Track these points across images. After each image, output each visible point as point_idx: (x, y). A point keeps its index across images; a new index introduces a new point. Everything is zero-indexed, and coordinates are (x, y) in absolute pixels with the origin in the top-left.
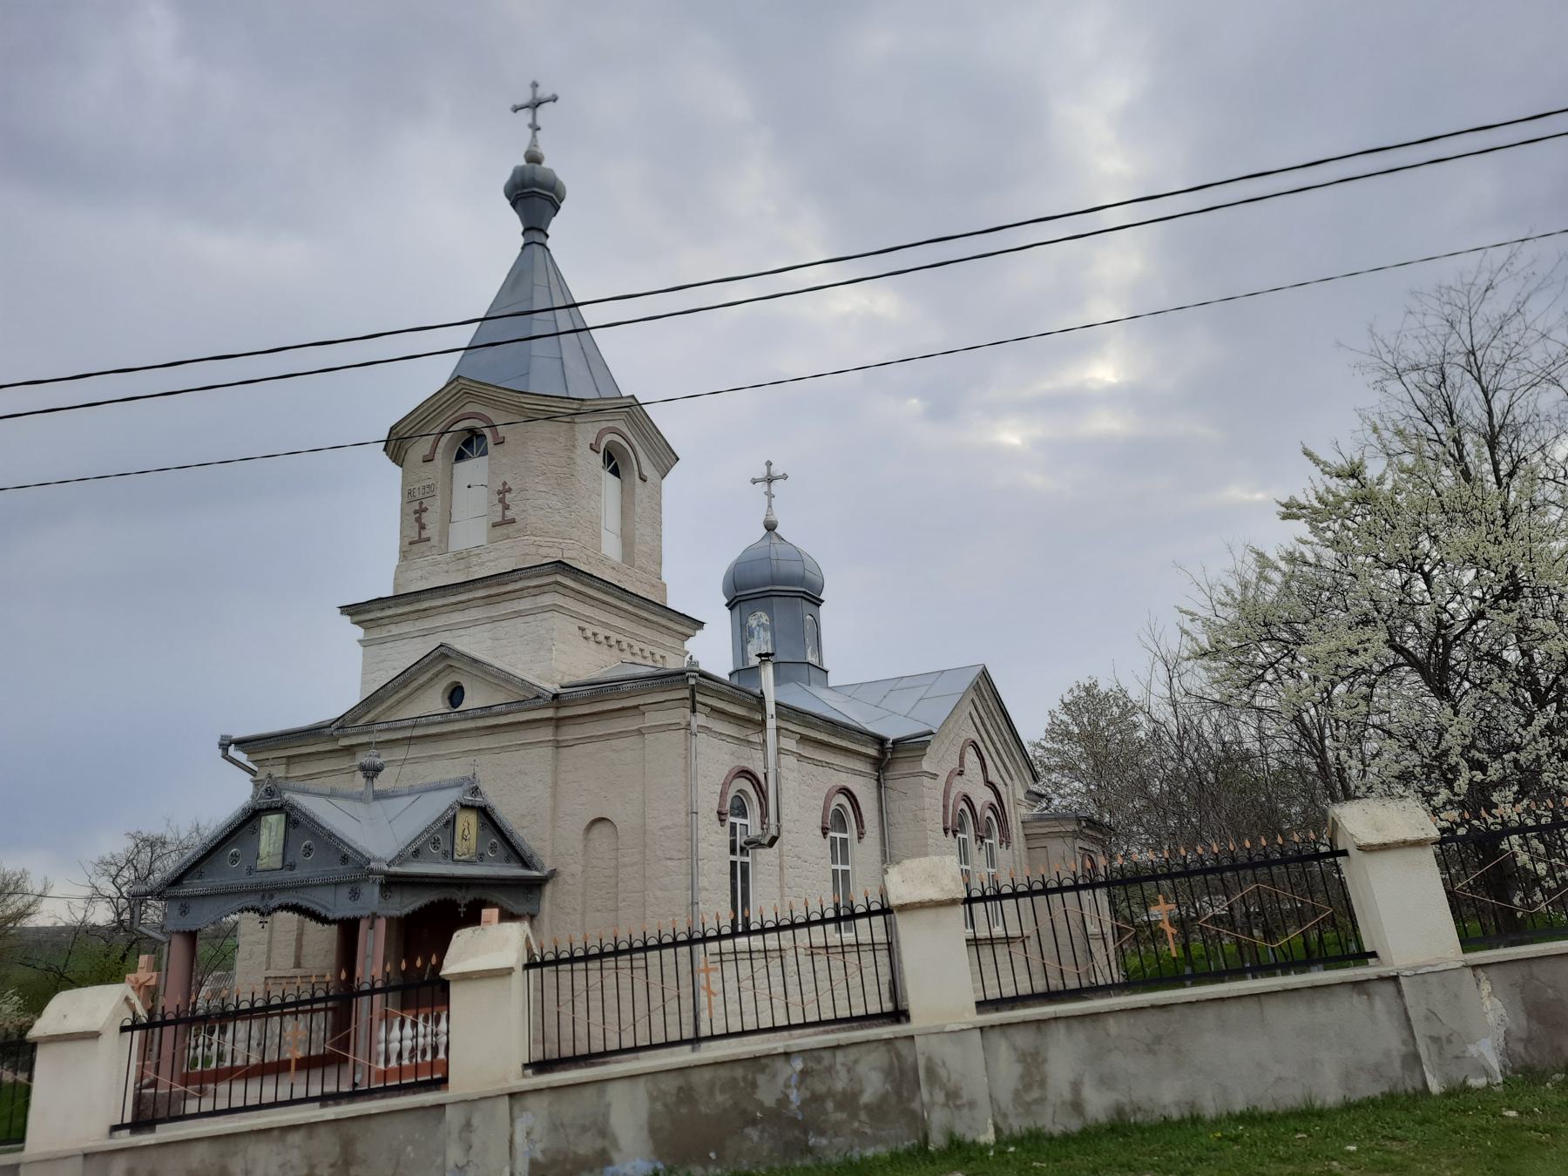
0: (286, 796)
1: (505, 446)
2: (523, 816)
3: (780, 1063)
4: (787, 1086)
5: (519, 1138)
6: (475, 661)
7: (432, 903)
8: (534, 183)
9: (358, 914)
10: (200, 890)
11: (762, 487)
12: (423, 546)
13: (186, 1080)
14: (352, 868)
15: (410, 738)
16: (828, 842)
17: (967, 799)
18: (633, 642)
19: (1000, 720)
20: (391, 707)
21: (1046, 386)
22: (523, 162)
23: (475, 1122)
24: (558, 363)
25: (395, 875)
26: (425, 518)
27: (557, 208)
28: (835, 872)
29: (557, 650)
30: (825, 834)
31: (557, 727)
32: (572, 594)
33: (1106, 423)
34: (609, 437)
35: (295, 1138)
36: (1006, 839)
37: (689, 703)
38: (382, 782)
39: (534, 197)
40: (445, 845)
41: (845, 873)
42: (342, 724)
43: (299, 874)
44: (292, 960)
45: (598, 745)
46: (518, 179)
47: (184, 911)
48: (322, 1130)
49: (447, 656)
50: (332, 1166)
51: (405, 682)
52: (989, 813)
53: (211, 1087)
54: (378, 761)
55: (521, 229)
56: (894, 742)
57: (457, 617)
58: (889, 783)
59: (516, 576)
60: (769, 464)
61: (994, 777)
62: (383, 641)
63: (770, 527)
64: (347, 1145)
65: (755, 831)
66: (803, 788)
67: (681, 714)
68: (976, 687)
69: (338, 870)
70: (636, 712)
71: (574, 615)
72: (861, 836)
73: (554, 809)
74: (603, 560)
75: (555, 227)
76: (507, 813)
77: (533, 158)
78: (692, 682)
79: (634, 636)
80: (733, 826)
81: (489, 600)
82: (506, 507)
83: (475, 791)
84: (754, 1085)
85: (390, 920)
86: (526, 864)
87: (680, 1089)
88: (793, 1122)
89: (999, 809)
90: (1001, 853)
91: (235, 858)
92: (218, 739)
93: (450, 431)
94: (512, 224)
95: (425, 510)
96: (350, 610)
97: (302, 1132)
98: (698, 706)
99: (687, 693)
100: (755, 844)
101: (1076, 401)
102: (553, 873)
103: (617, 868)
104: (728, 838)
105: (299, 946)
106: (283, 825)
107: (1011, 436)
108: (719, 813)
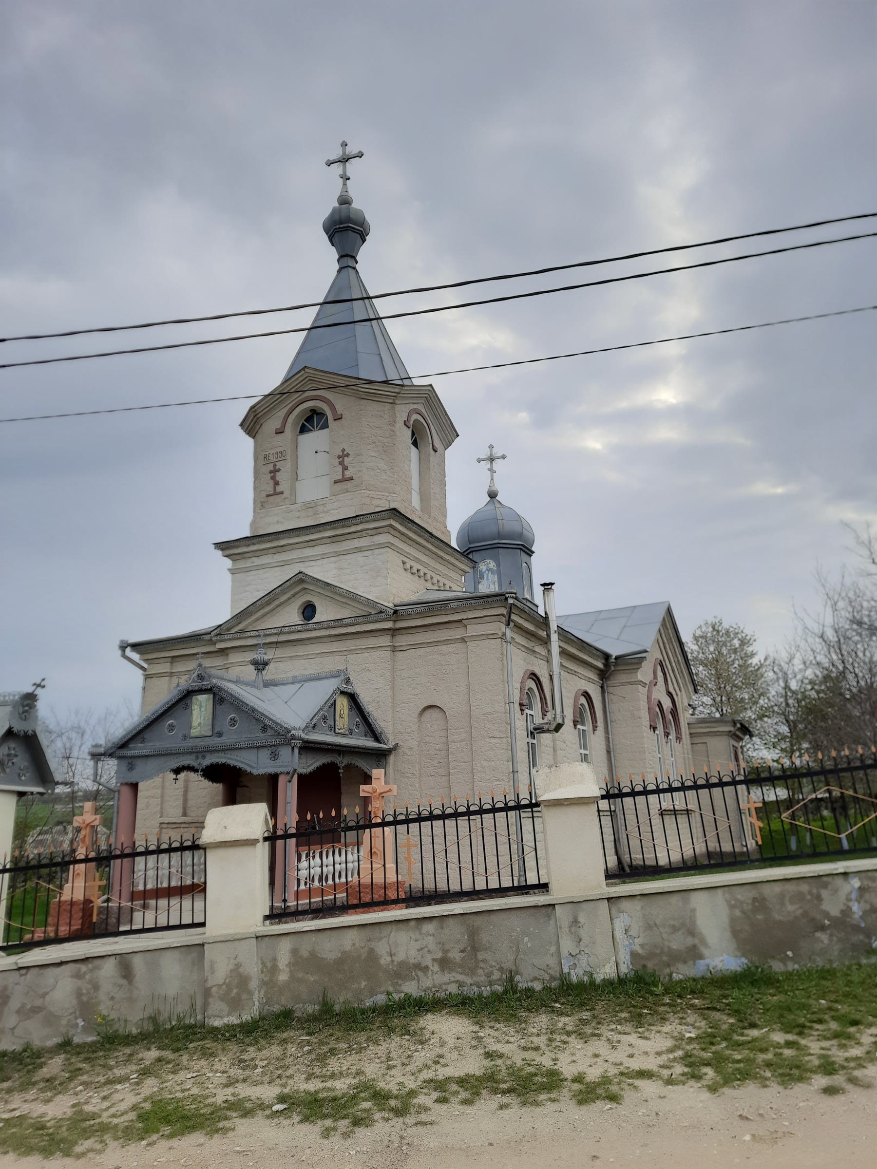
0: (214, 681)
1: (343, 421)
3: (839, 881)
4: (849, 900)
5: (619, 934)
6: (328, 584)
7: (324, 764)
8: (349, 220)
9: (278, 770)
10: (145, 752)
11: (486, 465)
13: (133, 896)
14: (278, 737)
15: (277, 643)
17: (660, 705)
18: (434, 575)
20: (257, 620)
21: (624, 404)
22: (337, 205)
23: (582, 919)
24: (378, 358)
25: (307, 742)
26: (279, 476)
27: (364, 240)
30: (575, 726)
32: (398, 535)
33: (666, 434)
34: (415, 416)
35: (429, 927)
36: (679, 738)
37: (504, 619)
38: (270, 673)
39: (346, 230)
40: (330, 722)
42: (220, 631)
43: (227, 739)
44: (181, 811)
46: (337, 217)
47: (131, 768)
48: (451, 921)
50: (462, 951)
51: (270, 601)
53: (152, 902)
54: (266, 658)
55: (337, 257)
56: (616, 658)
57: (308, 552)
58: (611, 690)
59: (358, 520)
61: (671, 690)
62: (247, 570)
63: (493, 495)
64: (473, 934)
67: (499, 627)
69: (259, 737)
71: (400, 552)
72: (595, 728)
75: (365, 255)
76: (365, 699)
77: (345, 201)
78: (511, 601)
79: (434, 570)
81: (334, 539)
82: (345, 468)
83: (348, 681)
84: (819, 898)
85: (300, 776)
86: (377, 739)
87: (755, 899)
88: (856, 929)
89: (674, 712)
90: (675, 744)
91: (171, 728)
92: (118, 643)
93: (301, 406)
94: (331, 254)
95: (279, 470)
96: (222, 546)
97: (435, 923)
99: (504, 611)
101: (644, 416)
102: (396, 746)
105: (185, 800)
106: (211, 702)
107: (594, 442)
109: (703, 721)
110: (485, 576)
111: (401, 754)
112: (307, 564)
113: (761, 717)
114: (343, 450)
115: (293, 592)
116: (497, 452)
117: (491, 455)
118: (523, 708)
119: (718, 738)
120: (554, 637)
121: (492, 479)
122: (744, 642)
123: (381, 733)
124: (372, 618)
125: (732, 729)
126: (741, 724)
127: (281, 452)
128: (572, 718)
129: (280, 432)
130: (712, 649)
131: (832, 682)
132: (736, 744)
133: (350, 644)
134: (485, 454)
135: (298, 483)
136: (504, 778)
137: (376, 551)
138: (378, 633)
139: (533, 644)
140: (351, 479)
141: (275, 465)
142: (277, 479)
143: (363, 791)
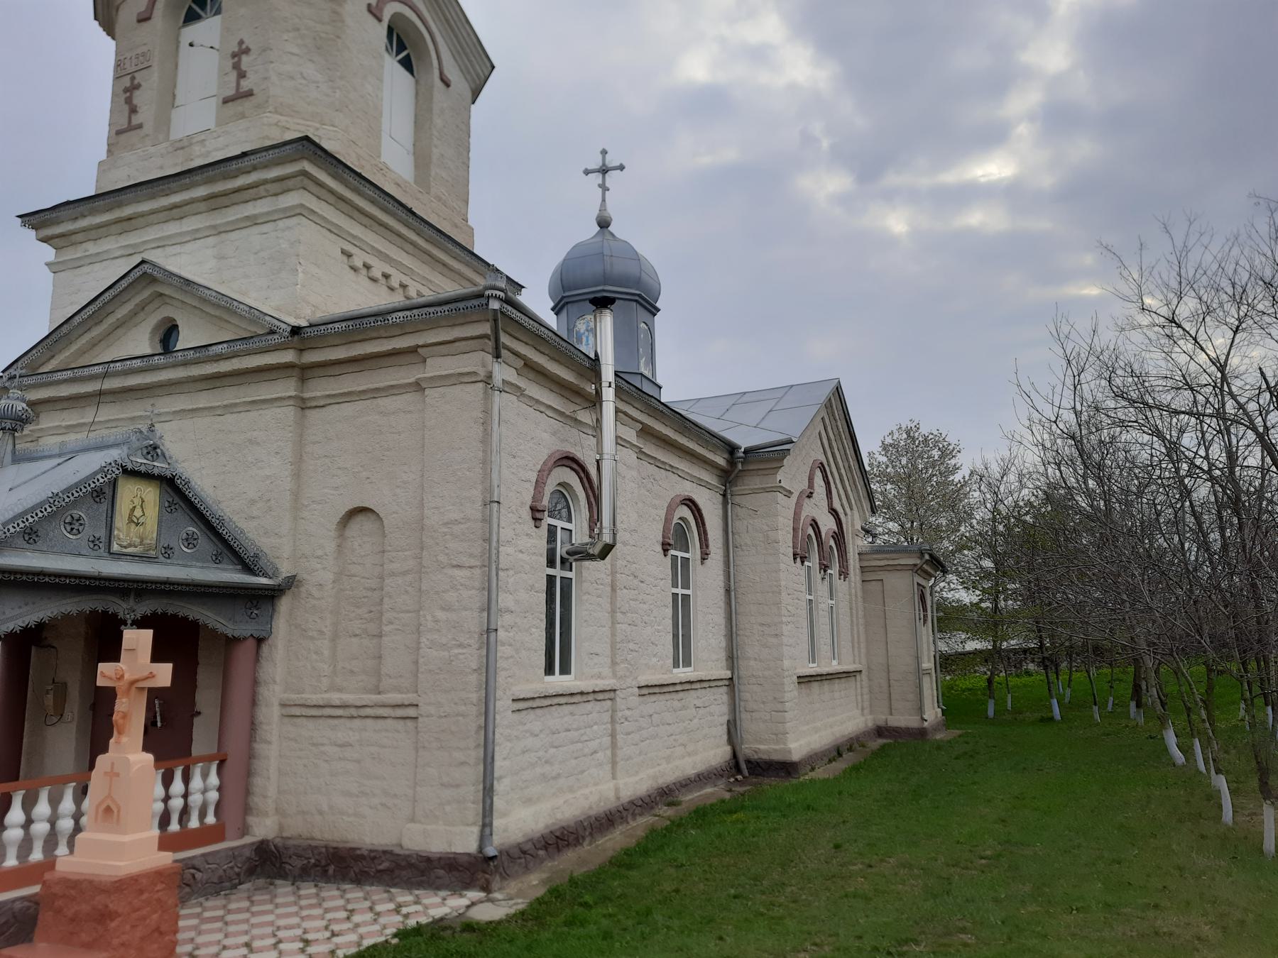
2: (253, 502)
12: (133, 136)
15: (101, 393)
16: (669, 557)
17: (815, 524)
19: (847, 443)
26: (138, 97)
28: (675, 595)
29: (300, 270)
30: (665, 551)
31: (303, 380)
32: (332, 199)
36: (844, 573)
37: (490, 344)
41: (686, 598)
45: (360, 405)
49: (154, 280)
52: (832, 543)
56: (746, 452)
57: (172, 228)
58: (737, 499)
60: (604, 152)
61: (837, 505)
62: (77, 265)
63: (604, 224)
65: (581, 536)
66: (641, 496)
67: (477, 361)
68: (828, 405)
70: (408, 358)
72: (705, 556)
73: (296, 495)
74: (383, 169)
78: (495, 305)
80: (552, 531)
81: (215, 202)
82: (242, 75)
83: (153, 450)
86: (248, 568)
89: (839, 536)
90: (839, 584)
95: (138, 87)
96: (34, 220)
98: (504, 352)
99: (486, 328)
100: (581, 554)
103: (382, 578)
104: (543, 546)
108: (533, 509)
109: (879, 551)
110: (584, 339)
111: (303, 595)
112: (170, 250)
113: (960, 548)
114: (241, 42)
115: (137, 299)
116: (612, 160)
117: (604, 165)
118: (538, 515)
119: (898, 574)
120: (609, 394)
121: (604, 200)
122: (946, 453)
123: (256, 556)
124: (257, 344)
125: (918, 562)
126: (931, 555)
127: (143, 54)
128: (660, 539)
129: (144, 19)
130: (904, 461)
131: (1056, 499)
132: (923, 582)
133: (229, 395)
134: (596, 163)
135: (174, 111)
136: (471, 641)
137: (281, 224)
138: (274, 375)
139: (573, 407)
140: (250, 94)
141: (133, 78)
142: (135, 101)
143: (104, 676)
